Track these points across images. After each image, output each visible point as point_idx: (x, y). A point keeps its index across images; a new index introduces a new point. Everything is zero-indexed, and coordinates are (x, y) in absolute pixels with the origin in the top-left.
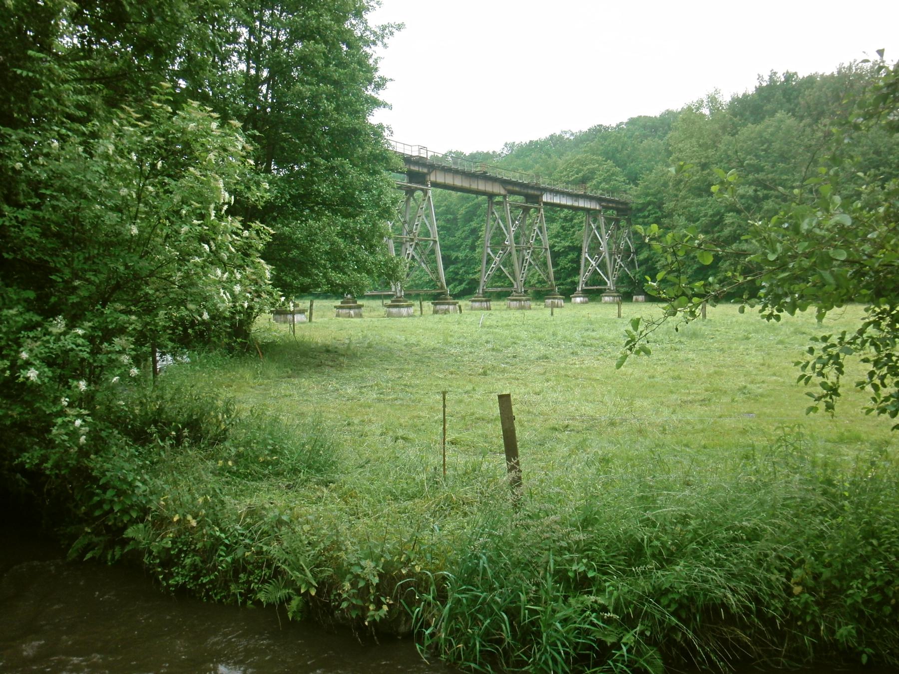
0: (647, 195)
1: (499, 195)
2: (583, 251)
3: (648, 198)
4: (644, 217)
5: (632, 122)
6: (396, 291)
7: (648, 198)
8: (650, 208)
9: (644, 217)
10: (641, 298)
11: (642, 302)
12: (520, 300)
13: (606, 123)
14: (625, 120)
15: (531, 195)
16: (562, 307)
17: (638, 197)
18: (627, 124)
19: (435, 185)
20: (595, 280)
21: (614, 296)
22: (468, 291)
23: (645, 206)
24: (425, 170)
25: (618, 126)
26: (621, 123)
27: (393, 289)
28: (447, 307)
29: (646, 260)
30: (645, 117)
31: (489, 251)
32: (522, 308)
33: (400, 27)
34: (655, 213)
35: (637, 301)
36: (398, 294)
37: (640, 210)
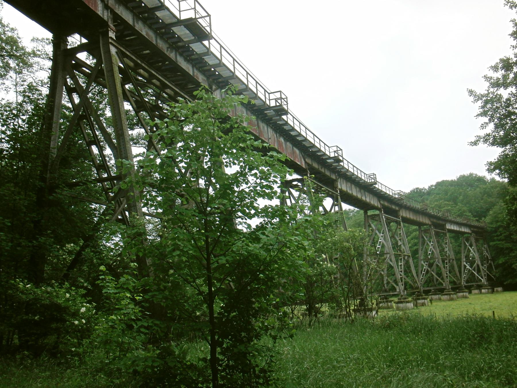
0: (497, 222)
1: (426, 224)
2: (462, 261)
3: (499, 224)
4: (497, 236)
5: (438, 184)
6: (400, 292)
7: (499, 224)
8: (501, 229)
9: (497, 236)
10: (500, 289)
11: (501, 291)
12: (450, 294)
13: (421, 187)
14: (434, 184)
15: (439, 224)
16: (468, 298)
17: (491, 223)
18: (435, 186)
19: (406, 220)
20: (472, 278)
21: (487, 289)
22: (441, 291)
23: (496, 230)
24: (397, 208)
25: (429, 187)
26: (432, 186)
27: (398, 290)
28: (423, 301)
29: (504, 264)
30: (446, 181)
31: (465, 263)
32: (452, 299)
33: (471, 92)
34: (505, 233)
35: (497, 291)
36: (402, 293)
37: (496, 231)
